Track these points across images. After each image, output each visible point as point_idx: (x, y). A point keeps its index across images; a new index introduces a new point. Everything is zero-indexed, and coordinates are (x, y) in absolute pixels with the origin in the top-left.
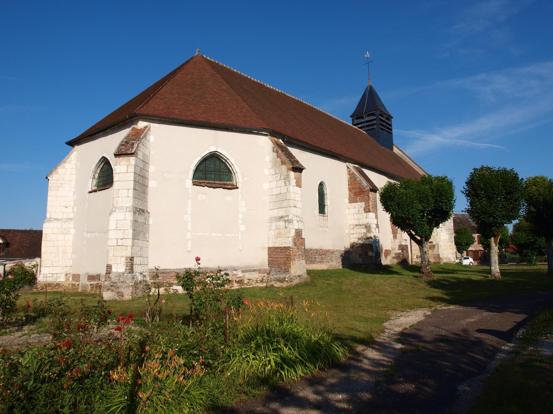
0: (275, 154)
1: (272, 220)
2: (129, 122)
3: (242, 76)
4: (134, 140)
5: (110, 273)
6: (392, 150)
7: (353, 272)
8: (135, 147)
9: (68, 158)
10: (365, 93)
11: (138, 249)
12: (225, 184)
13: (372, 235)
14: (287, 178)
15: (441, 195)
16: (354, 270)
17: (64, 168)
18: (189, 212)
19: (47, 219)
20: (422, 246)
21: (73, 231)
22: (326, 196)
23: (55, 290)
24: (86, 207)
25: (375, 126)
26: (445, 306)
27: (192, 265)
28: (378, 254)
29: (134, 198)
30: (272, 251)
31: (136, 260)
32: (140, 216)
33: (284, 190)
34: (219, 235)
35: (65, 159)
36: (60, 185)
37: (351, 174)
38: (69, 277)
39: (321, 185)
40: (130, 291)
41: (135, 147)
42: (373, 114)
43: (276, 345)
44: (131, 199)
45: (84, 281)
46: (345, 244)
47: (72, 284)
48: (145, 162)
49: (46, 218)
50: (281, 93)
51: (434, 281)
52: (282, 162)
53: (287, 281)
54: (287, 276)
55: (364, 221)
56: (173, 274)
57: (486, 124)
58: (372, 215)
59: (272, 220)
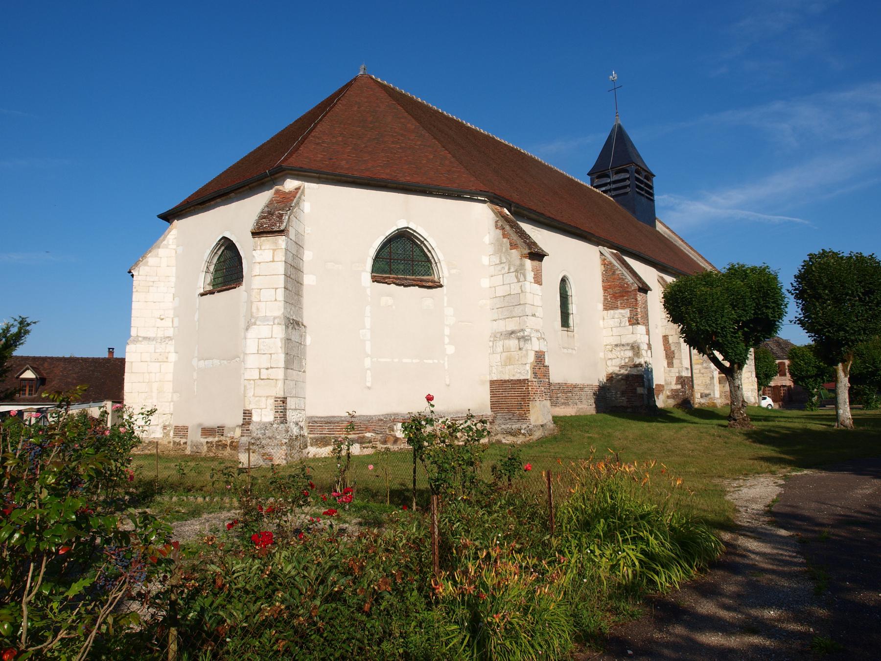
0: (499, 232)
1: (495, 336)
2: (269, 181)
3: (431, 109)
4: (283, 210)
5: (249, 424)
6: (654, 226)
7: (619, 420)
8: (286, 221)
9: (164, 240)
10: (610, 137)
11: (292, 384)
12: (422, 281)
13: (642, 361)
14: (520, 271)
15: (766, 295)
16: (620, 417)
17: (157, 256)
18: (368, 324)
19: (132, 338)
20: (732, 376)
21: (173, 357)
22: (570, 299)
23: (147, 452)
24: (196, 319)
25: (628, 190)
26: (794, 470)
27: (420, 407)
28: (651, 392)
29: (286, 302)
30: (497, 387)
31: (291, 403)
32: (294, 332)
33: (515, 289)
34: (414, 361)
35: (158, 241)
36: (151, 284)
37: (606, 265)
38: (170, 431)
39: (564, 281)
40: (283, 453)
41: (286, 221)
42: (625, 171)
43: (634, 533)
44: (282, 304)
45: (195, 437)
46: (598, 376)
47: (174, 443)
48: (299, 246)
49: (130, 336)
50: (488, 136)
51: (755, 432)
52: (511, 244)
53: (524, 434)
54: (524, 426)
55: (630, 339)
56: (345, 424)
57: (782, 184)
58: (641, 329)
59: (495, 336)
